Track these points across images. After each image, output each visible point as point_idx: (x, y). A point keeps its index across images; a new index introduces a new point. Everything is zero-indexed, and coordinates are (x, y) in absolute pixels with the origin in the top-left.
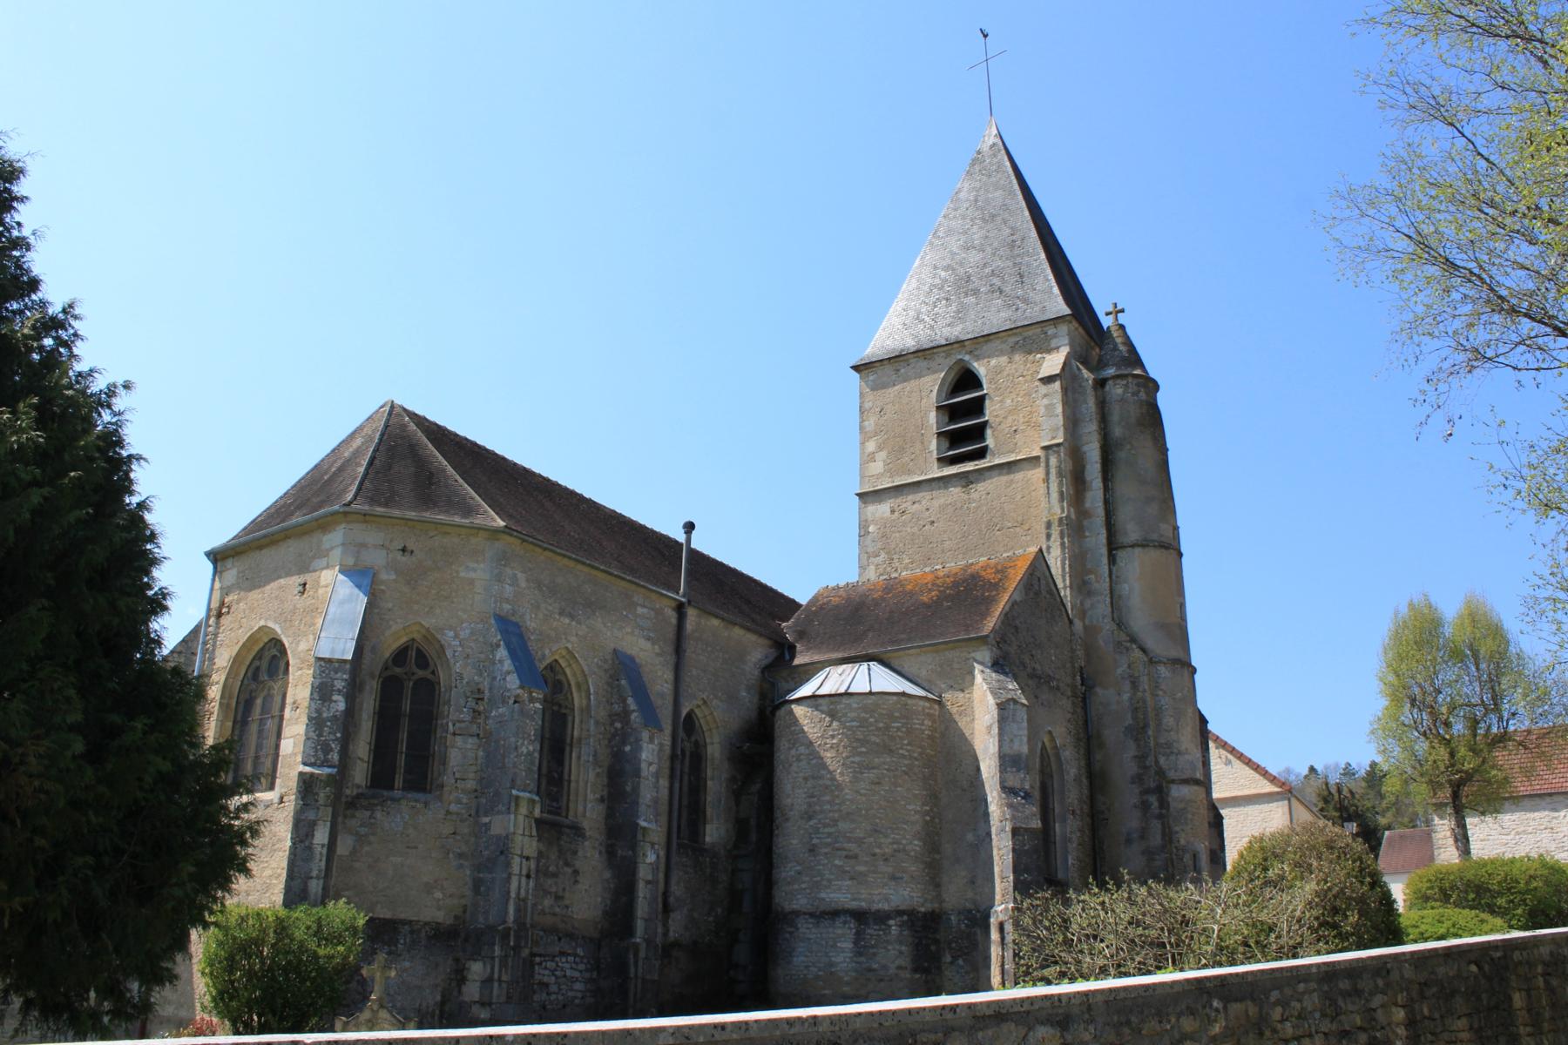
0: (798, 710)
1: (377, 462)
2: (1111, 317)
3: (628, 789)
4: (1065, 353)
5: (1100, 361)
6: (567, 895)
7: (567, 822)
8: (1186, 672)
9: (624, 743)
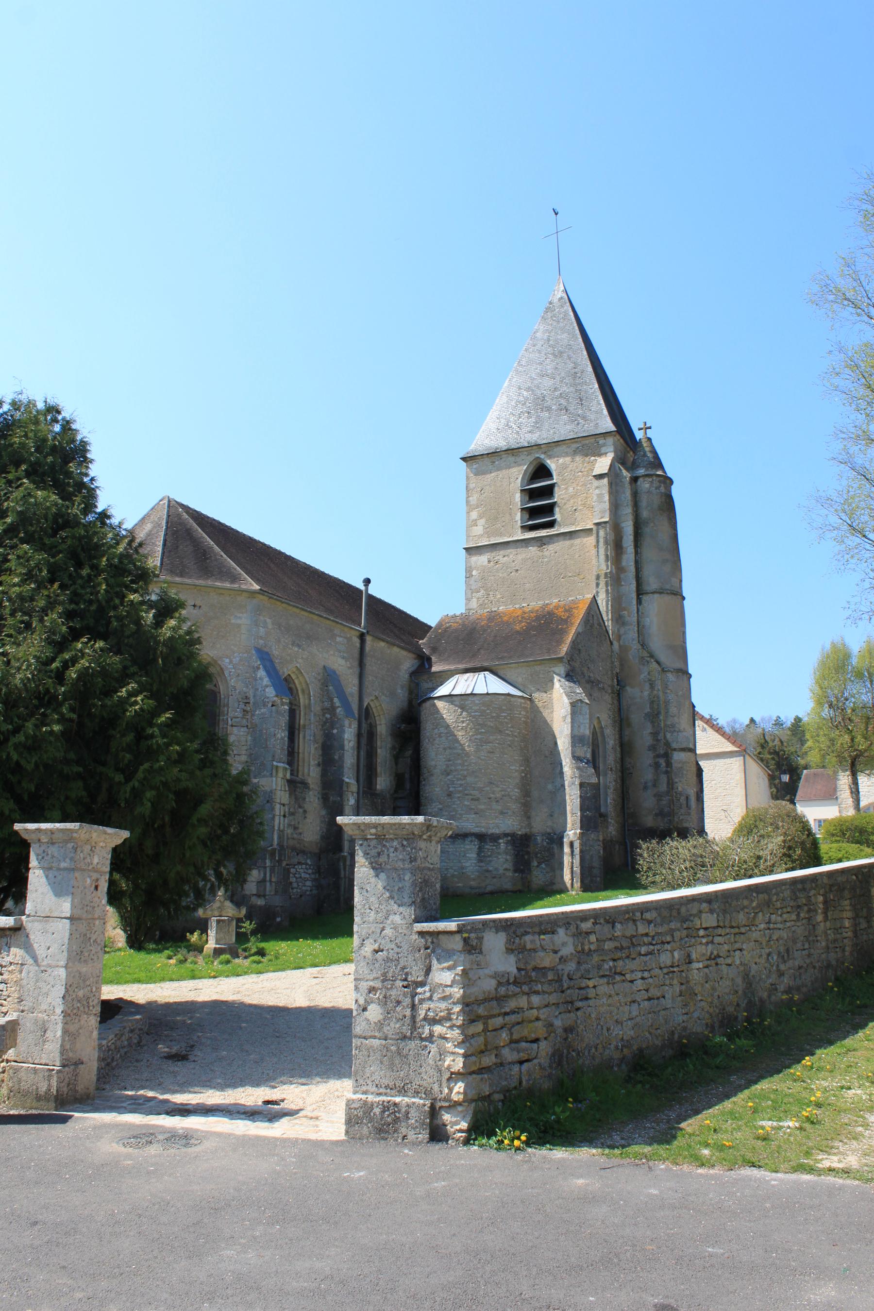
0: (440, 704)
1: (168, 543)
3: (336, 757)
4: (611, 458)
5: (634, 462)
6: (300, 826)
7: (298, 779)
8: (685, 678)
9: (333, 728)
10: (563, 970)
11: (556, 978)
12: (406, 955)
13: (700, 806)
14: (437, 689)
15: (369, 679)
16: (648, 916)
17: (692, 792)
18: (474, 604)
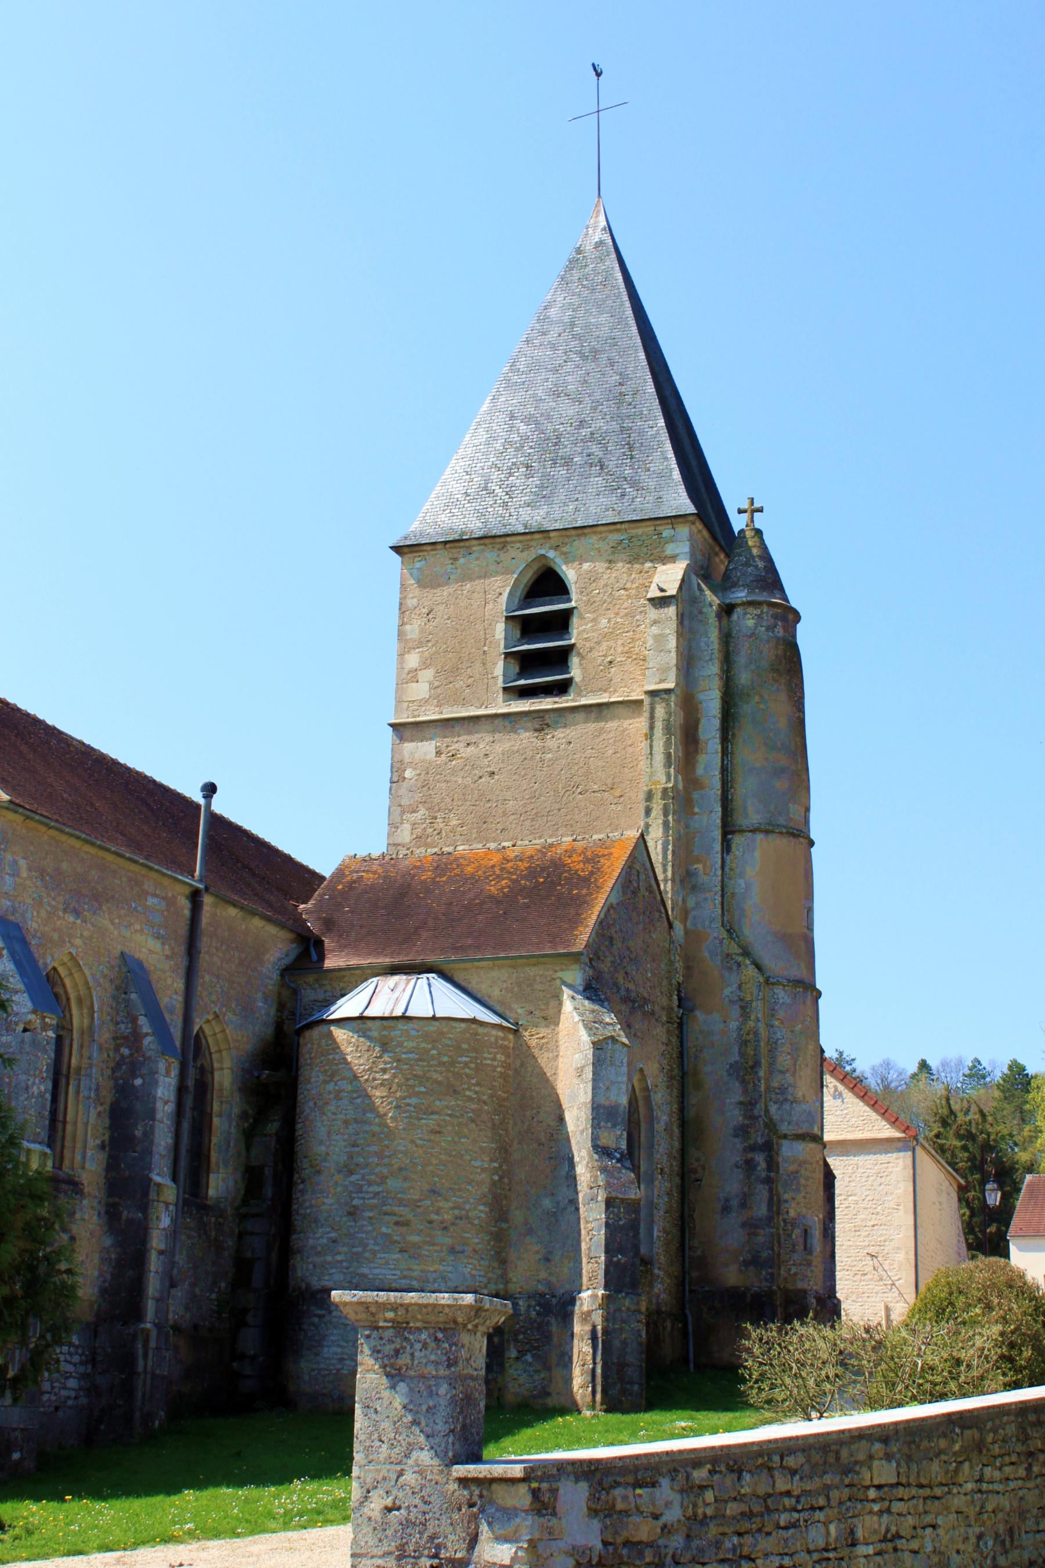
0: (340, 1034)
2: (745, 517)
3: (138, 1133)
5: (726, 576)
9: (135, 1077)
10: (666, 1547)
11: (657, 1560)
12: (437, 1516)
13: (828, 1248)
14: (333, 1003)
15: (205, 979)
16: (791, 1461)
17: (815, 1219)
18: (405, 835)
